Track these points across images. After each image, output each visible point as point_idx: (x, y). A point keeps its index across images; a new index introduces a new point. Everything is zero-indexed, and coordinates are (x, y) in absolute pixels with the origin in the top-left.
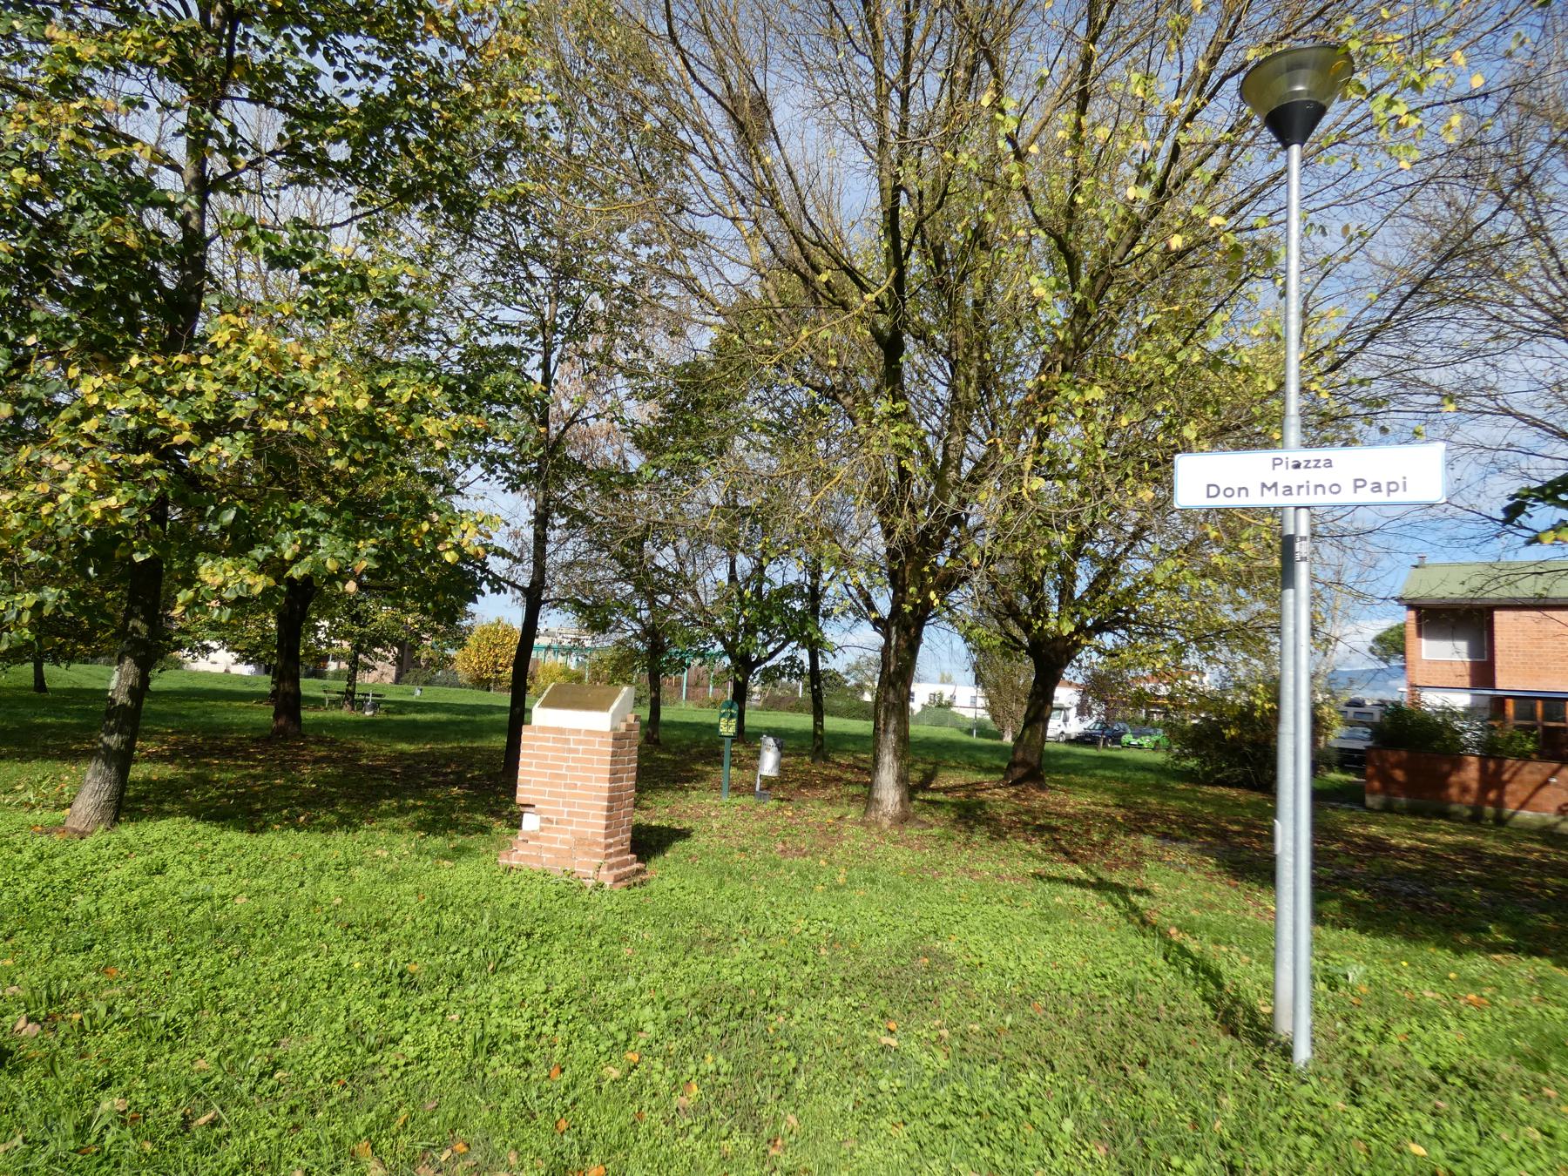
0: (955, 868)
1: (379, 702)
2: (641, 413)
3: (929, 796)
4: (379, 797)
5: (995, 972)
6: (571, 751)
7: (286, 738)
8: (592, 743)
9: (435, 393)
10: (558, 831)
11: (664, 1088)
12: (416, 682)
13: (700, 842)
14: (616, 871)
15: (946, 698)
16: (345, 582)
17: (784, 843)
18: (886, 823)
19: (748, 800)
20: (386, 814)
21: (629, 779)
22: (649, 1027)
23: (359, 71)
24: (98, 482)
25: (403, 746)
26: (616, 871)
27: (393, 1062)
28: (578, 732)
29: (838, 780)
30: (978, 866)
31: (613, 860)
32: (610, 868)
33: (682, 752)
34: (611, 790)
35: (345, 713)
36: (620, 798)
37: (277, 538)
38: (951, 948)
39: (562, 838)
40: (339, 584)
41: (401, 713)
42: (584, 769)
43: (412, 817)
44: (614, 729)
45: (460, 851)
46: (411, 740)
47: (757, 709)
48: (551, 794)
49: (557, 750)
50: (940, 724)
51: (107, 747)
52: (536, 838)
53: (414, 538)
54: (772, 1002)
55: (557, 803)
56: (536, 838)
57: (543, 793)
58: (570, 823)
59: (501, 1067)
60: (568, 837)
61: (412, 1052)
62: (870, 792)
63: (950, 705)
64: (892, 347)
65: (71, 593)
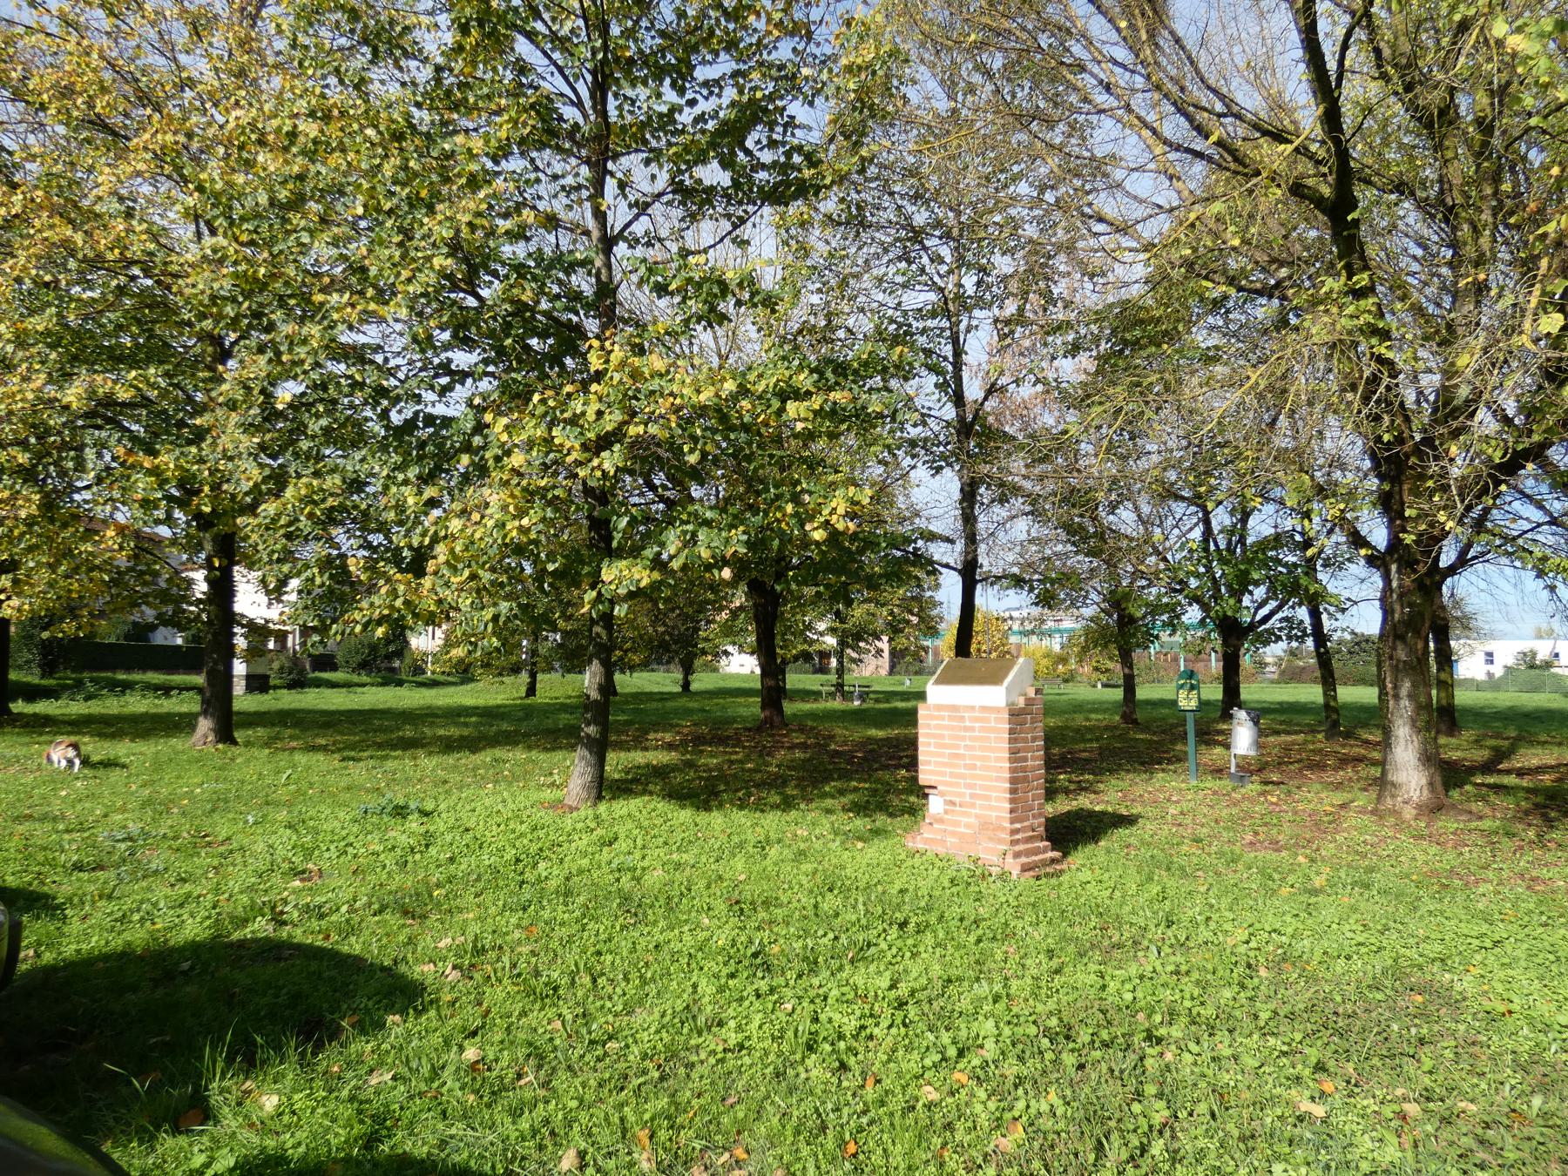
0: (1505, 874)
1: (867, 693)
2: (1073, 370)
3: (1491, 780)
4: (827, 779)
5: (1532, 1025)
6: (966, 729)
7: (772, 727)
8: (987, 720)
9: (802, 377)
10: (964, 814)
11: (984, 1121)
12: (907, 672)
13: (1145, 829)
14: (1024, 860)
15: (1540, 657)
16: (720, 570)
17: (1256, 833)
18: (1409, 813)
19: (1225, 784)
20: (824, 796)
21: (1035, 760)
22: (990, 1044)
23: (705, 92)
24: (516, 508)
25: (874, 732)
26: (1024, 860)
27: (712, 1047)
28: (972, 708)
29: (1359, 760)
30: (1545, 873)
31: (1019, 848)
32: (1017, 855)
33: (1163, 732)
34: (1012, 770)
35: (837, 704)
36: (1025, 779)
37: (663, 538)
38: (1466, 985)
39: (966, 822)
40: (716, 572)
41: (888, 701)
42: (982, 749)
43: (844, 800)
44: (1010, 705)
45: (876, 832)
46: (879, 725)
47: (1272, 682)
48: (952, 775)
49: (952, 728)
50: (1535, 690)
51: (588, 736)
52: (941, 821)
53: (778, 521)
54: (1162, 1031)
55: (958, 785)
56: (941, 821)
57: (943, 774)
58: (973, 805)
59: (816, 1070)
60: (972, 820)
61: (733, 1039)
62: (1384, 773)
63: (1548, 665)
64: (1338, 210)
65: (519, 605)
